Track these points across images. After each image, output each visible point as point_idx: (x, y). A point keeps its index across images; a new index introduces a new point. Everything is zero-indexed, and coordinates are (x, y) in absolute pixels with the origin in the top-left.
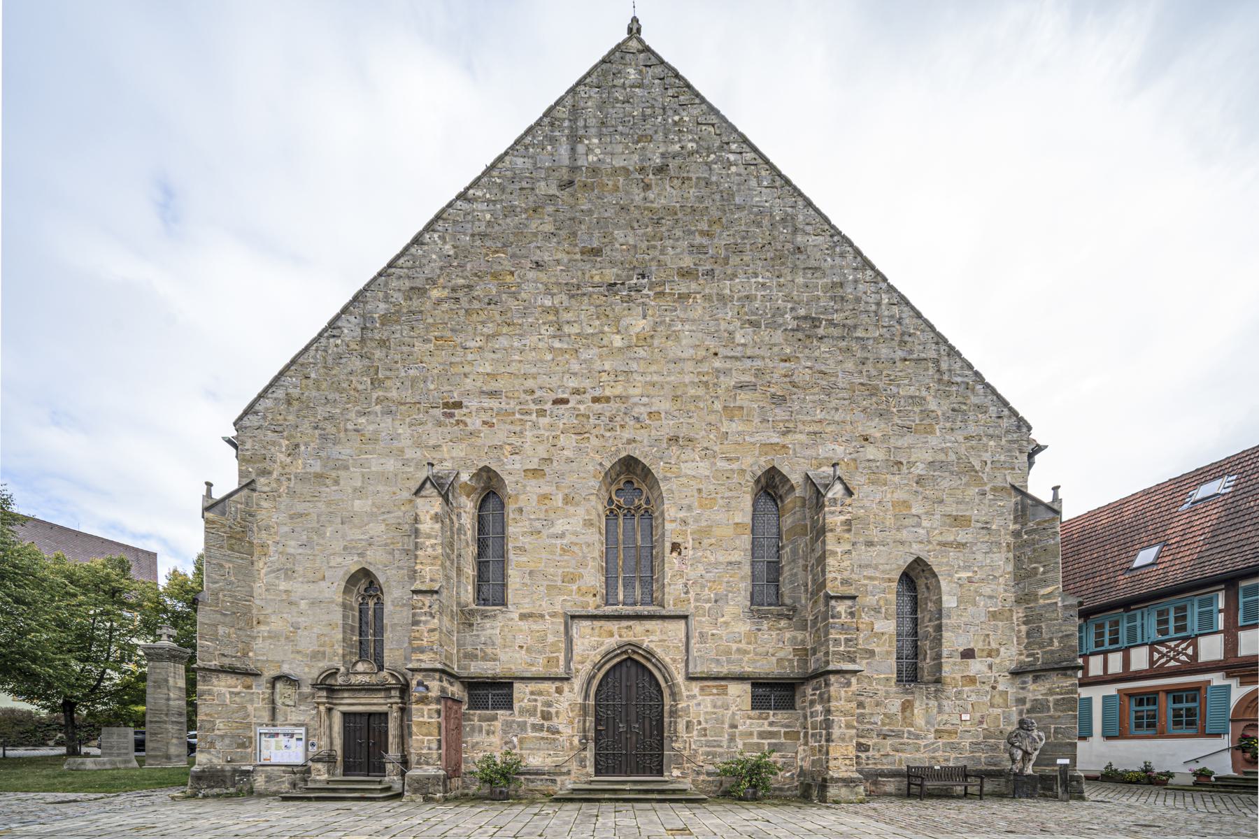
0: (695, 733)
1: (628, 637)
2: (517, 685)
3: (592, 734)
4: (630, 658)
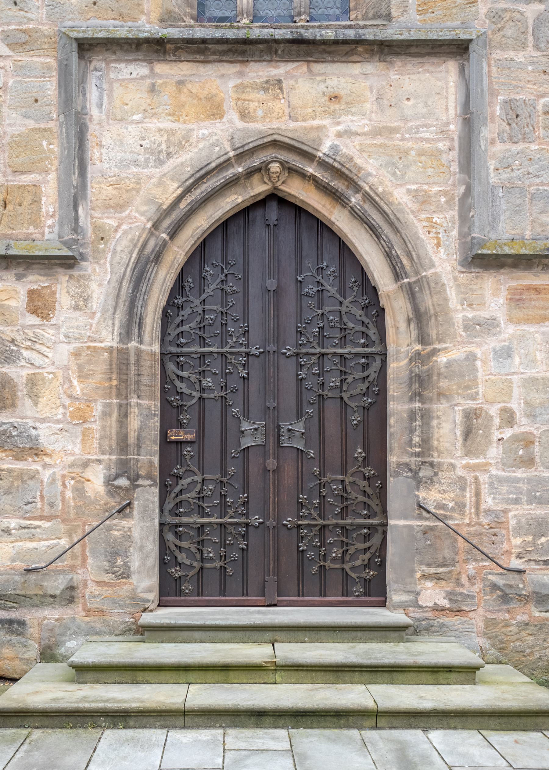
0: (494, 452)
1: (273, 118)
3: (150, 457)
4: (275, 198)
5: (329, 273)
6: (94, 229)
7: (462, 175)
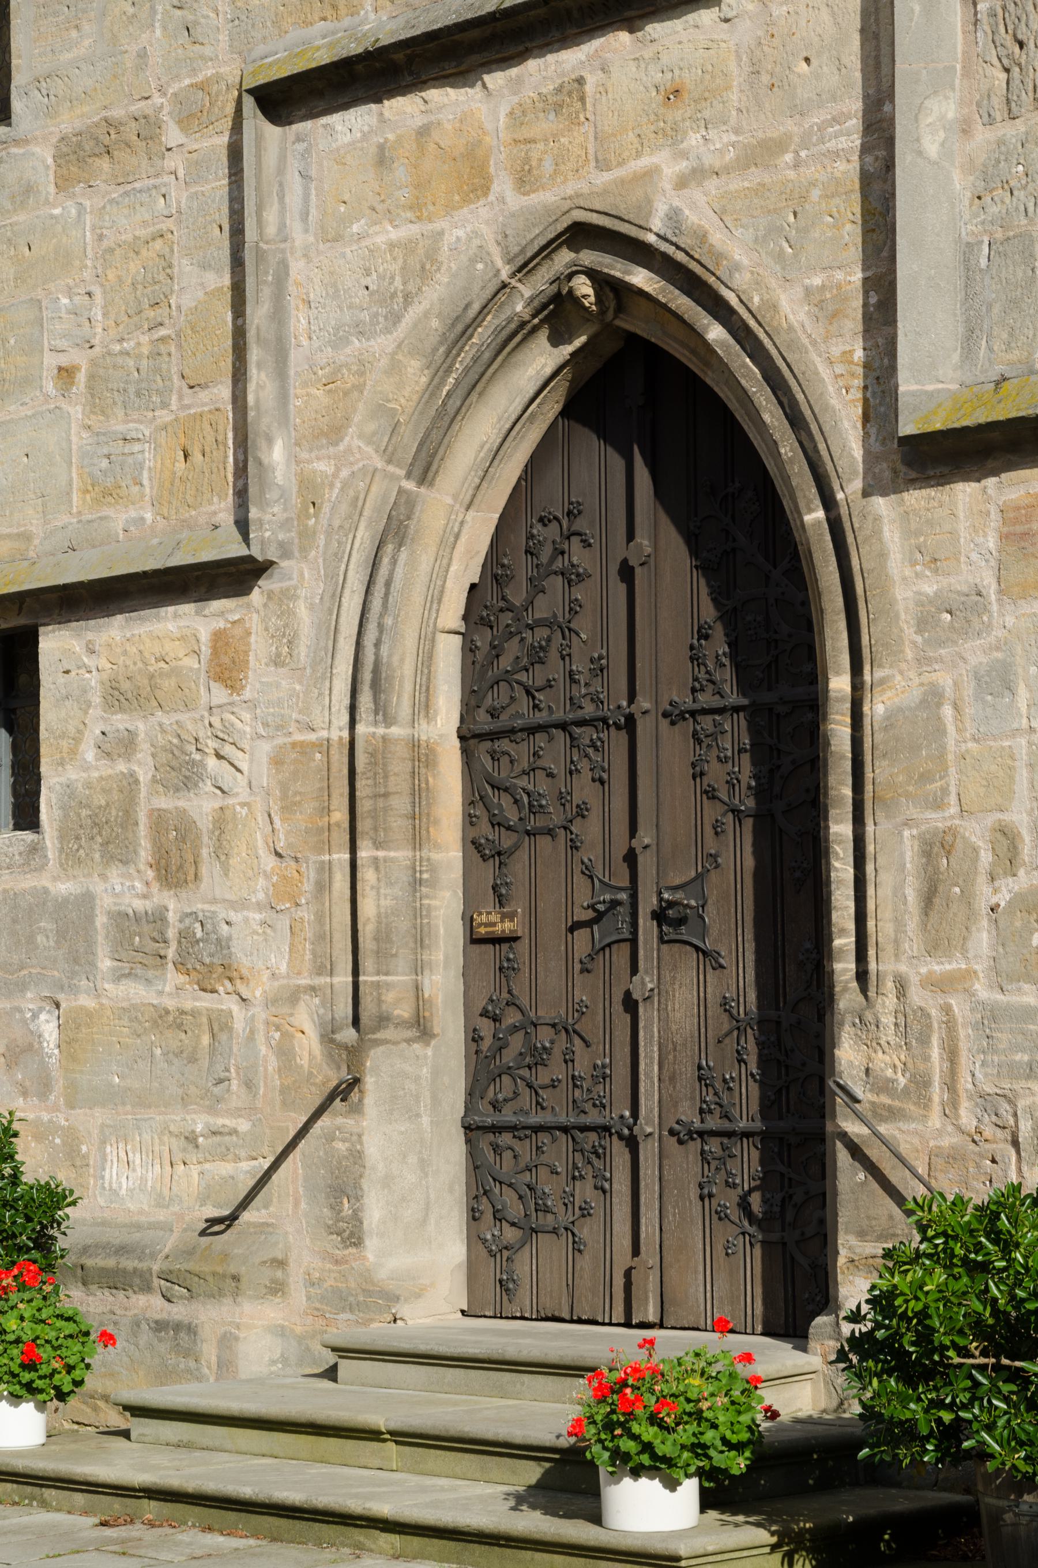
2: (57, 646)
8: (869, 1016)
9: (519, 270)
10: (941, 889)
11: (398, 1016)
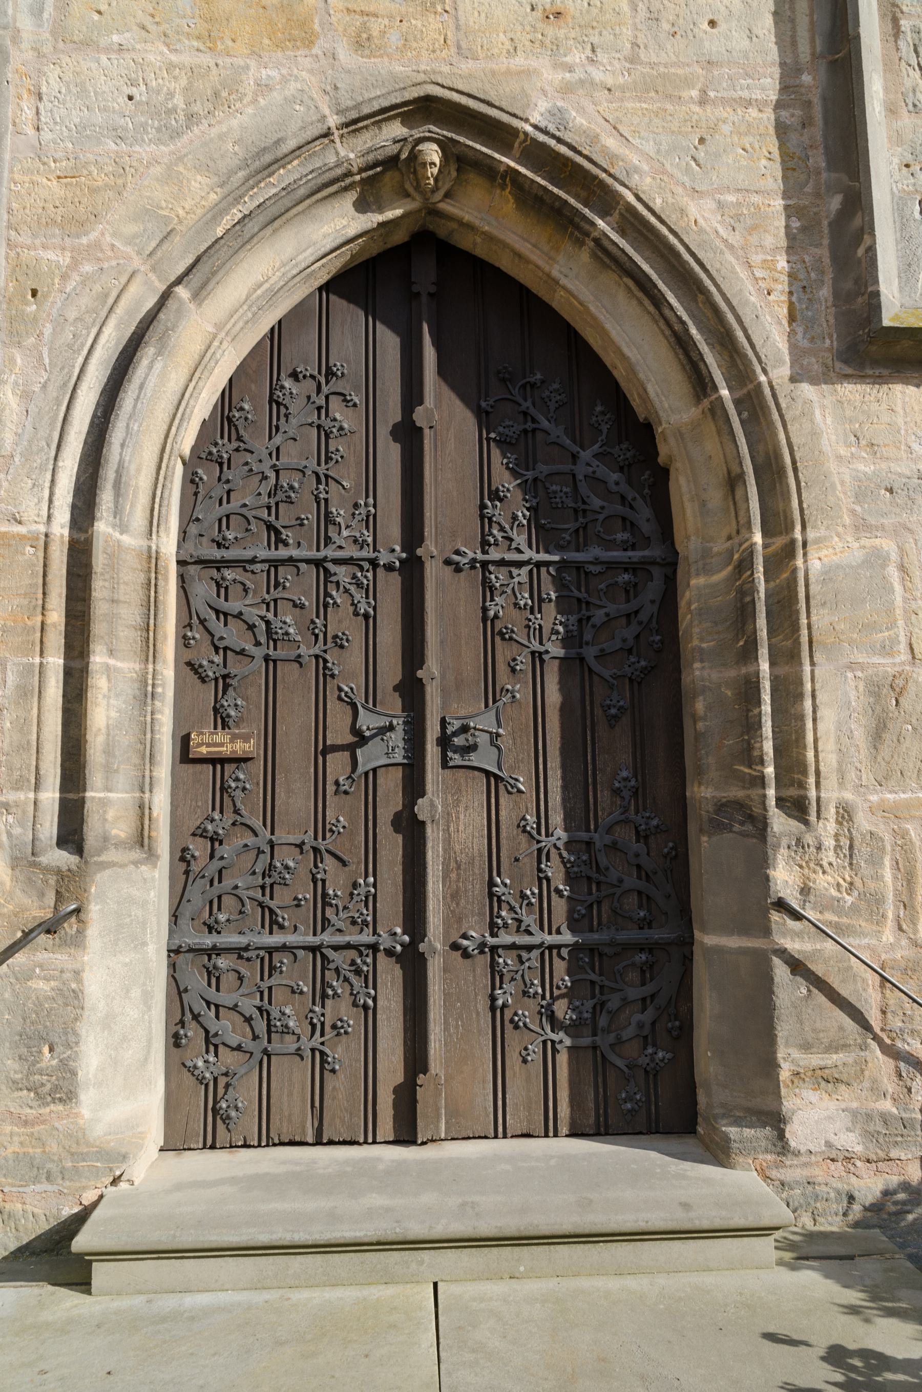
5: (547, 393)
6: (14, 271)
7: (833, 175)
8: (809, 839)
9: (347, 125)
10: (890, 725)
11: (116, 836)
